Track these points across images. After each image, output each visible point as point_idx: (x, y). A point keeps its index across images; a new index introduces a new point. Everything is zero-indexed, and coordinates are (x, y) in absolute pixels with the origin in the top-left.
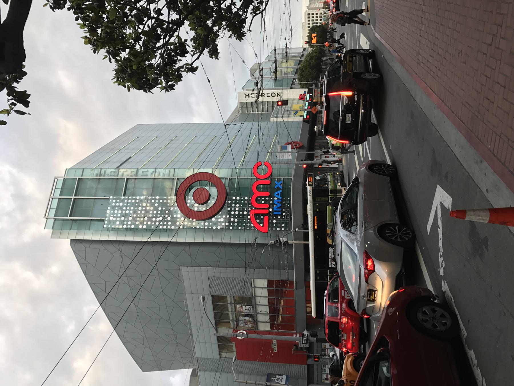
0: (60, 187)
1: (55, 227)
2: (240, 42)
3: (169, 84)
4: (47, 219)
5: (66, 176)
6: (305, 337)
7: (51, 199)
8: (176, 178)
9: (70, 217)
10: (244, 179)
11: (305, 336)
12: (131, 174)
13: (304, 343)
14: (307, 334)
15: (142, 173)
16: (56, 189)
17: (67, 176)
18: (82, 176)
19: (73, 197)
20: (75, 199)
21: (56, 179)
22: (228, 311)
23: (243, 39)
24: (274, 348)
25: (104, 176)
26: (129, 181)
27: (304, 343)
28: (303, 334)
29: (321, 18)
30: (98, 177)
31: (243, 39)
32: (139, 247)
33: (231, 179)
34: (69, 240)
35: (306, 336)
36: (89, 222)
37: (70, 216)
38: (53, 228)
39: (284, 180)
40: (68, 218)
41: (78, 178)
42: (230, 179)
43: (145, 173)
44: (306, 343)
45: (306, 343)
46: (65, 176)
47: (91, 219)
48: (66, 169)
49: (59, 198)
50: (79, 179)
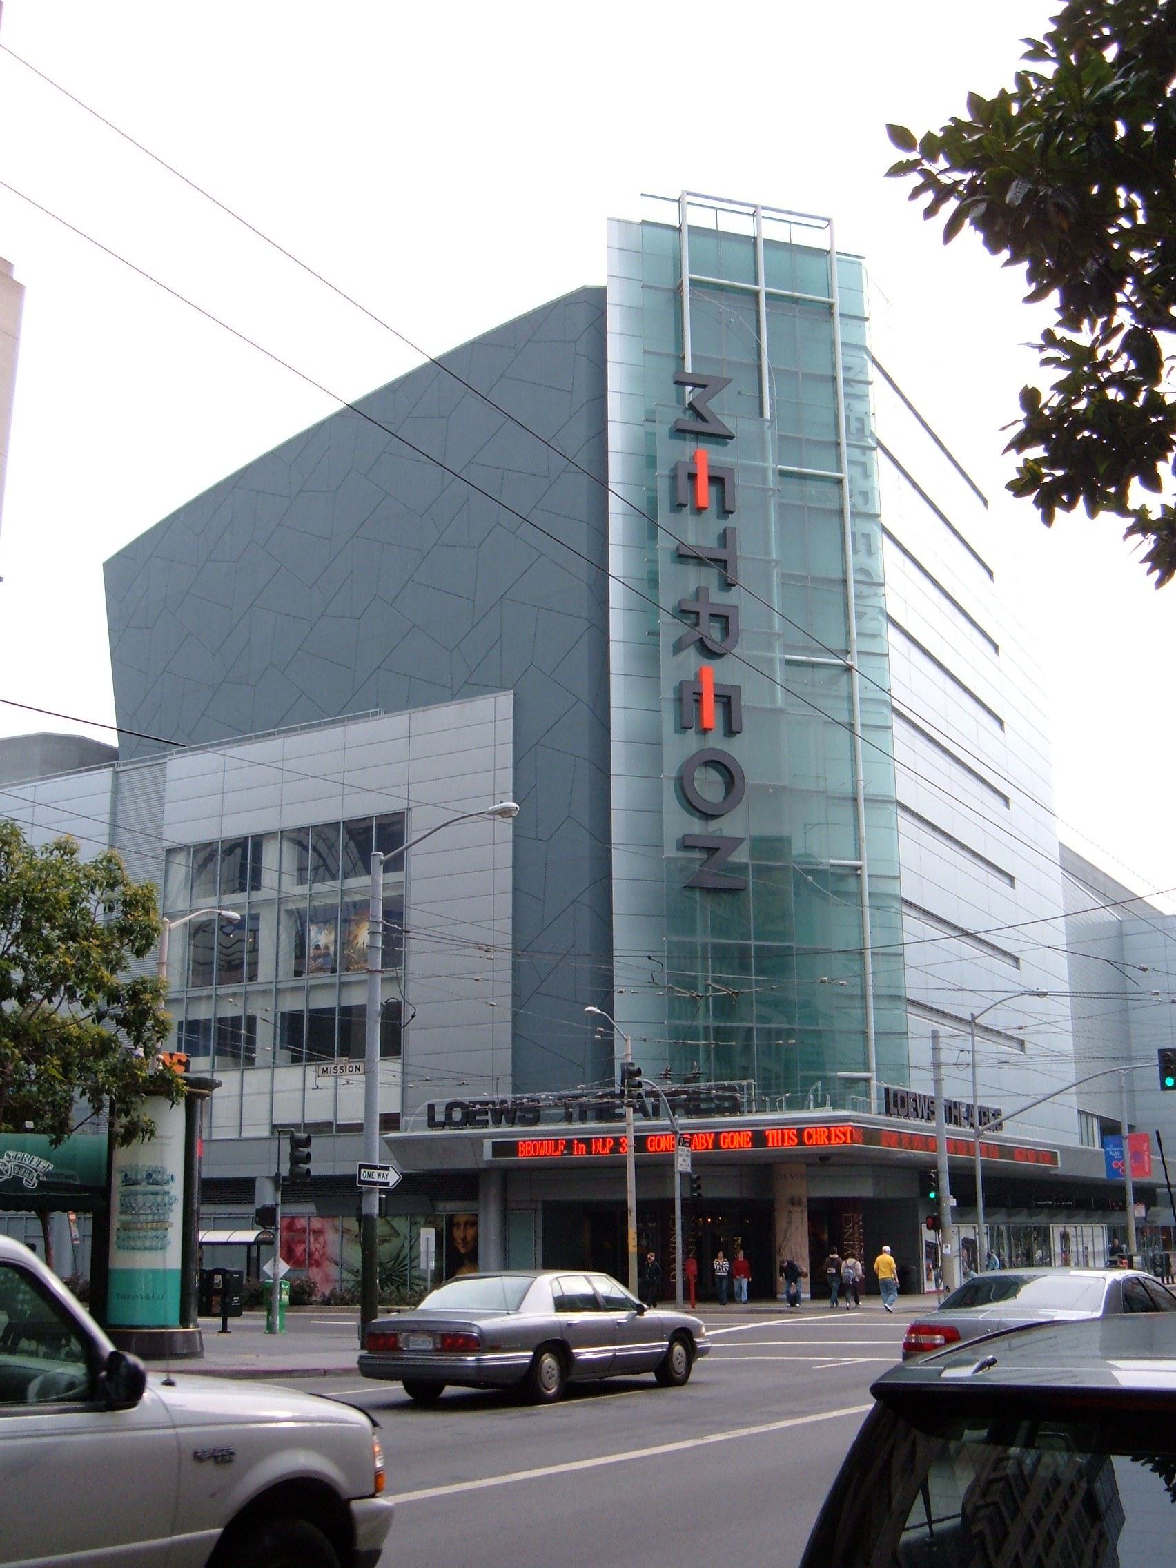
0: (797, 241)
1: (647, 228)
2: (1154, 586)
3: (1101, 472)
4: (679, 201)
5: (838, 256)
6: (379, 1175)
7: (751, 210)
8: (853, 661)
9: (691, 280)
10: (862, 927)
11: (383, 1176)
12: (855, 492)
13: (362, 1170)
14: (387, 1184)
15: (863, 535)
16: (788, 224)
17: (839, 260)
18: (842, 315)
19: (762, 288)
20: (756, 295)
21: (824, 224)
22: (346, 876)
23: (1150, 571)
24: (333, 1066)
25: (847, 395)
26: (832, 490)
27: (362, 1170)
28: (387, 1169)
29: (875, 1102)
30: (840, 375)
31: (1150, 571)
32: (581, 539)
33: (859, 872)
34: (597, 278)
35: (383, 1180)
36: (671, 349)
37: (692, 282)
38: (644, 223)
39: (862, 1084)
40: (687, 276)
41: (836, 300)
42: (859, 868)
43: (861, 542)
44: (362, 1178)
45: (362, 1178)
46: (838, 253)
47: (683, 358)
48: (863, 258)
49: (755, 239)
50: (831, 306)
